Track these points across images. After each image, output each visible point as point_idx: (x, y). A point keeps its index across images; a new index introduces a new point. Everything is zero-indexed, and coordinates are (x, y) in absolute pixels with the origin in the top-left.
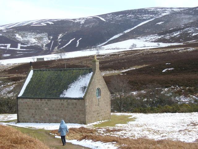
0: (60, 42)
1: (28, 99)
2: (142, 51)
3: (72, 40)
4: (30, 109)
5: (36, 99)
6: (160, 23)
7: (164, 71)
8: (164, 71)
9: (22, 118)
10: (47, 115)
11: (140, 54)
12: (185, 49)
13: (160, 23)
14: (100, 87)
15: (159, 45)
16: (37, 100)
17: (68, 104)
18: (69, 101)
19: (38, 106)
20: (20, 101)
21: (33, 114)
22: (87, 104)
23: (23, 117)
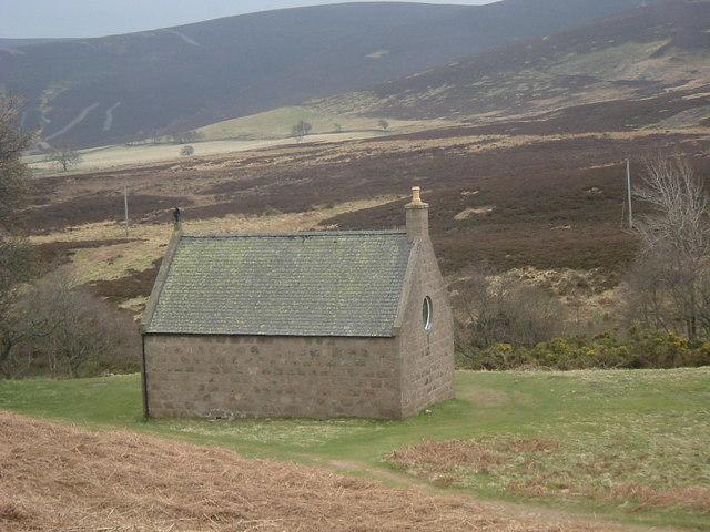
0: (49, 116)
1: (186, 339)
2: (347, 148)
3: (88, 109)
4: (191, 370)
5: (214, 340)
6: (377, 54)
7: (460, 216)
8: (460, 216)
9: (163, 402)
10: (257, 391)
11: (342, 157)
12: (485, 142)
13: (377, 54)
14: (431, 293)
15: (385, 125)
16: (246, 342)
17: (336, 353)
18: (339, 344)
19: (222, 360)
20: (152, 343)
21: (202, 388)
22: (403, 354)
23: (165, 397)
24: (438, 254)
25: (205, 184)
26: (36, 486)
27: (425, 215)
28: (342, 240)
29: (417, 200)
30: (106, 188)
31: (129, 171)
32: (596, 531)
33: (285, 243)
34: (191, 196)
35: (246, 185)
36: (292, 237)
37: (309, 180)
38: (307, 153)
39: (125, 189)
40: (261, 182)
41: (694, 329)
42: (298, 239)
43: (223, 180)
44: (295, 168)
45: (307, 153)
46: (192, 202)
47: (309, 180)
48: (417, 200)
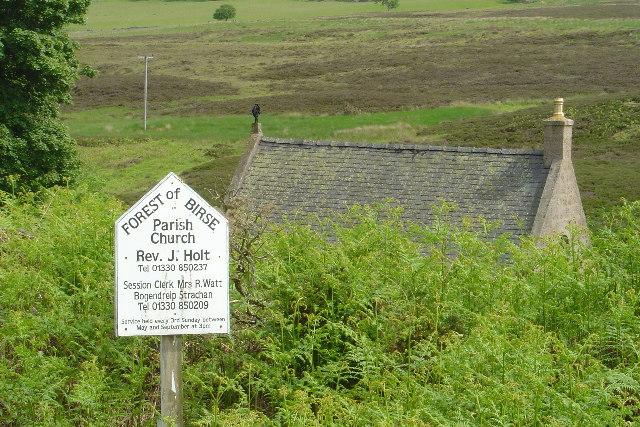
24: (582, 190)
25: (254, 65)
26: (345, 321)
27: (567, 134)
28: (461, 159)
29: (560, 115)
30: (111, 62)
31: (143, 38)
32: (21, 426)
33: (391, 158)
34: (234, 82)
35: (314, 71)
36: (399, 151)
37: (404, 69)
38: (404, 27)
39: (143, 65)
40: (335, 67)
41: (282, 77)
42: (408, 154)
43: (280, 61)
44: (385, 48)
45: (404, 27)
46: (235, 91)
47: (404, 69)
48: (560, 115)
